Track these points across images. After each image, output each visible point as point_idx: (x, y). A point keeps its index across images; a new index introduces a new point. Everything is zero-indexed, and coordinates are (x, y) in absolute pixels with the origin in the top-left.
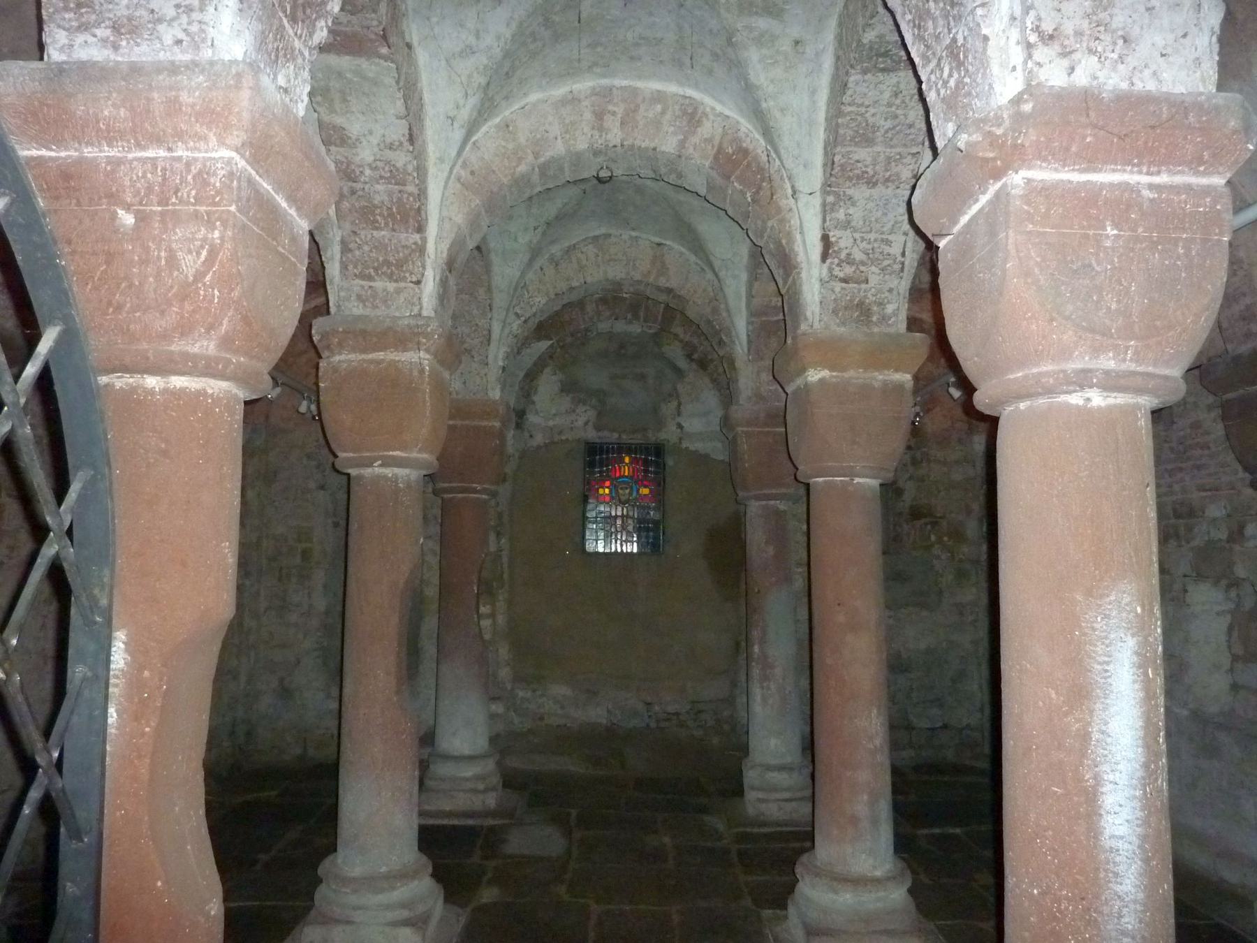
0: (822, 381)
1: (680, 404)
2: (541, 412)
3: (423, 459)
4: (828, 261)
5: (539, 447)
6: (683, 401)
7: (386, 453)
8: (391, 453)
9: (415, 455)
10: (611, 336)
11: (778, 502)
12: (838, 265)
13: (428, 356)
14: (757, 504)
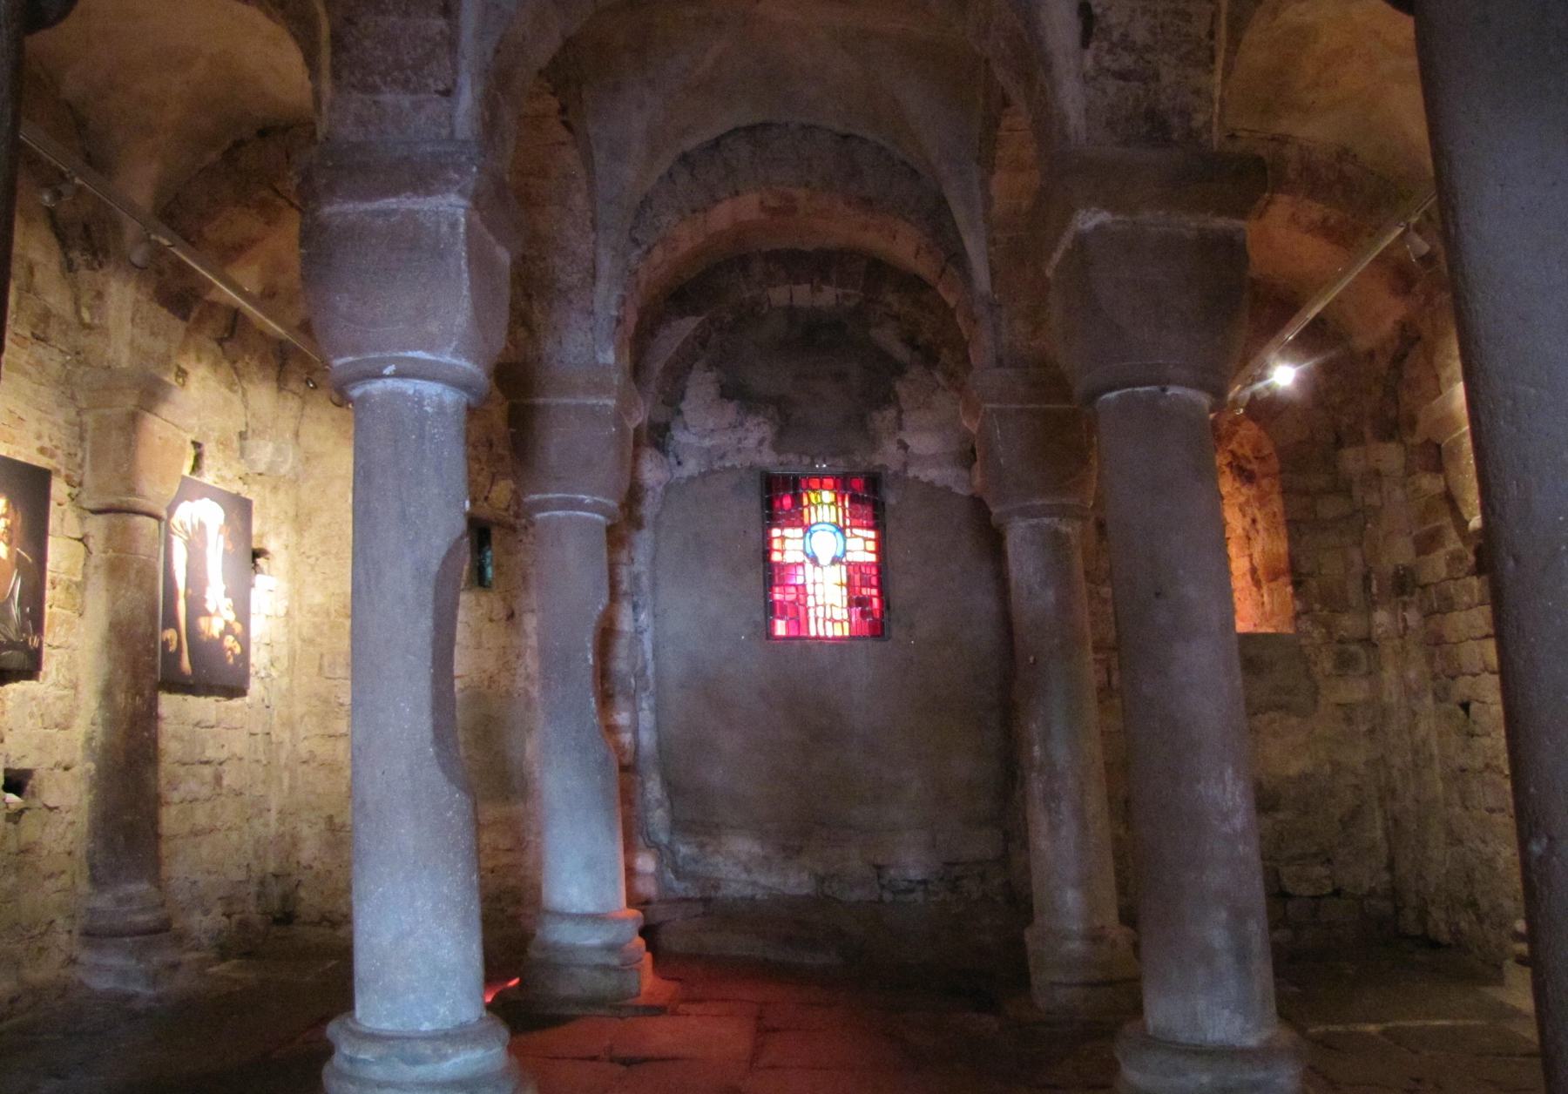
0: (1099, 228)
1: (900, 412)
2: (692, 426)
3: (460, 366)
4: (1093, 45)
5: (691, 479)
6: (904, 408)
7: (401, 354)
8: (410, 354)
9: (447, 359)
10: (791, 312)
11: (1056, 519)
12: (1110, 51)
13: (463, 202)
14: (1023, 524)
